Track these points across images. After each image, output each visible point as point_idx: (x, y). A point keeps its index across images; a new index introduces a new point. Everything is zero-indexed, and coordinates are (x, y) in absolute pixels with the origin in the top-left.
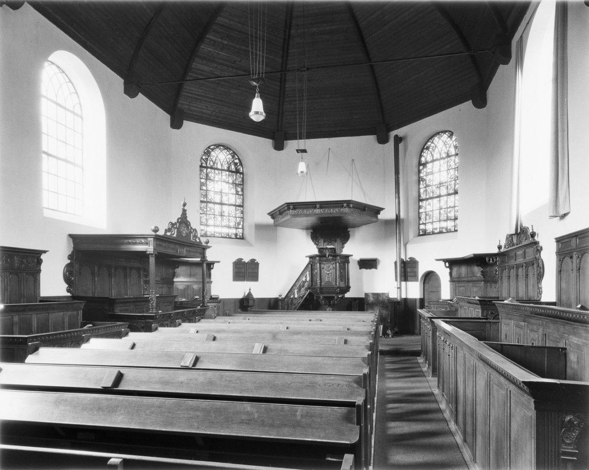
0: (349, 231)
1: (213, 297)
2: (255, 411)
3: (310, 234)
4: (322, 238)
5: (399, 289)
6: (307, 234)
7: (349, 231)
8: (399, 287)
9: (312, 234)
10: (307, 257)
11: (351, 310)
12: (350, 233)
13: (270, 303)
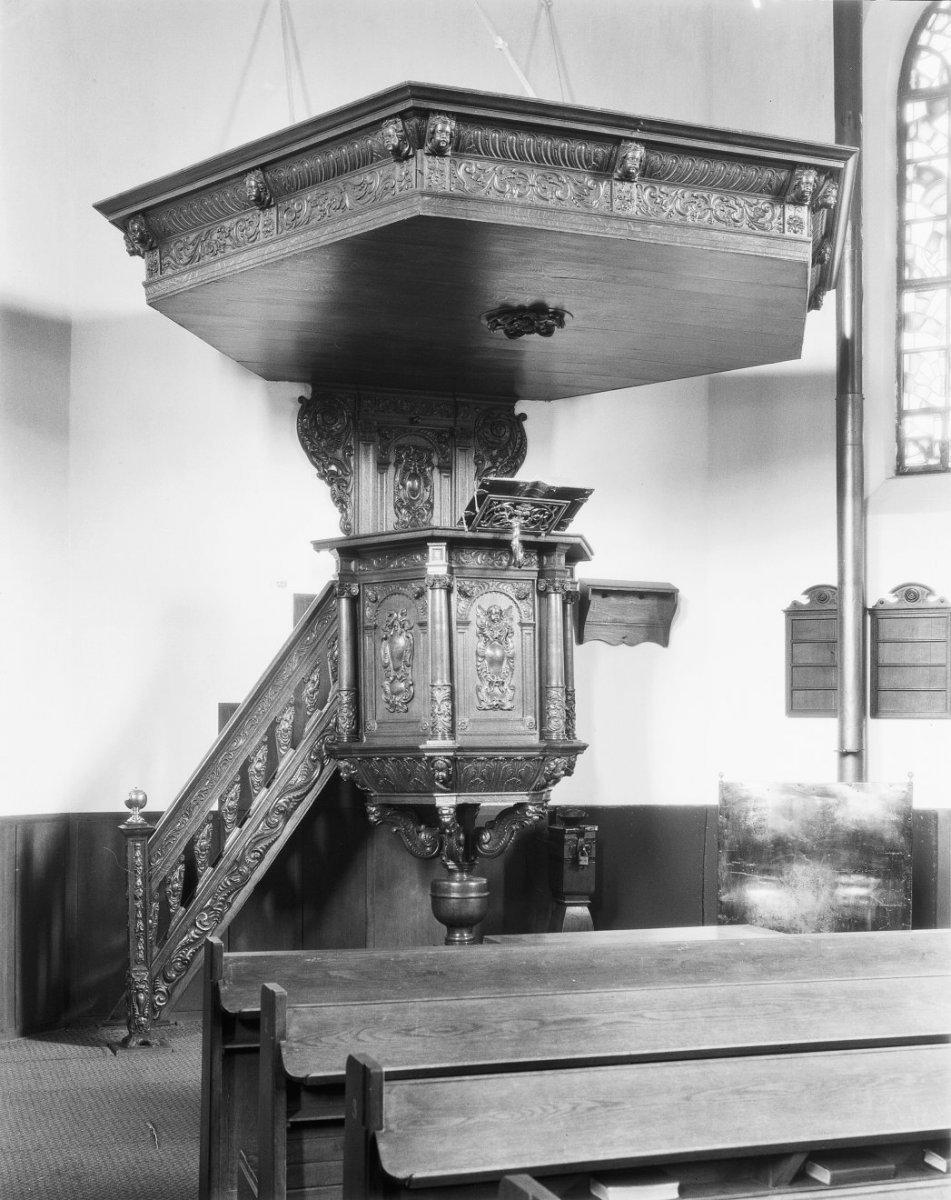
0: (523, 417)
1: (934, 16)
2: (387, 682)
3: (296, 407)
4: (367, 445)
5: (850, 761)
6: (275, 408)
7: (523, 417)
8: (850, 746)
9: (307, 408)
10: (319, 545)
11: (703, 924)
12: (527, 425)
13: (27, 857)
